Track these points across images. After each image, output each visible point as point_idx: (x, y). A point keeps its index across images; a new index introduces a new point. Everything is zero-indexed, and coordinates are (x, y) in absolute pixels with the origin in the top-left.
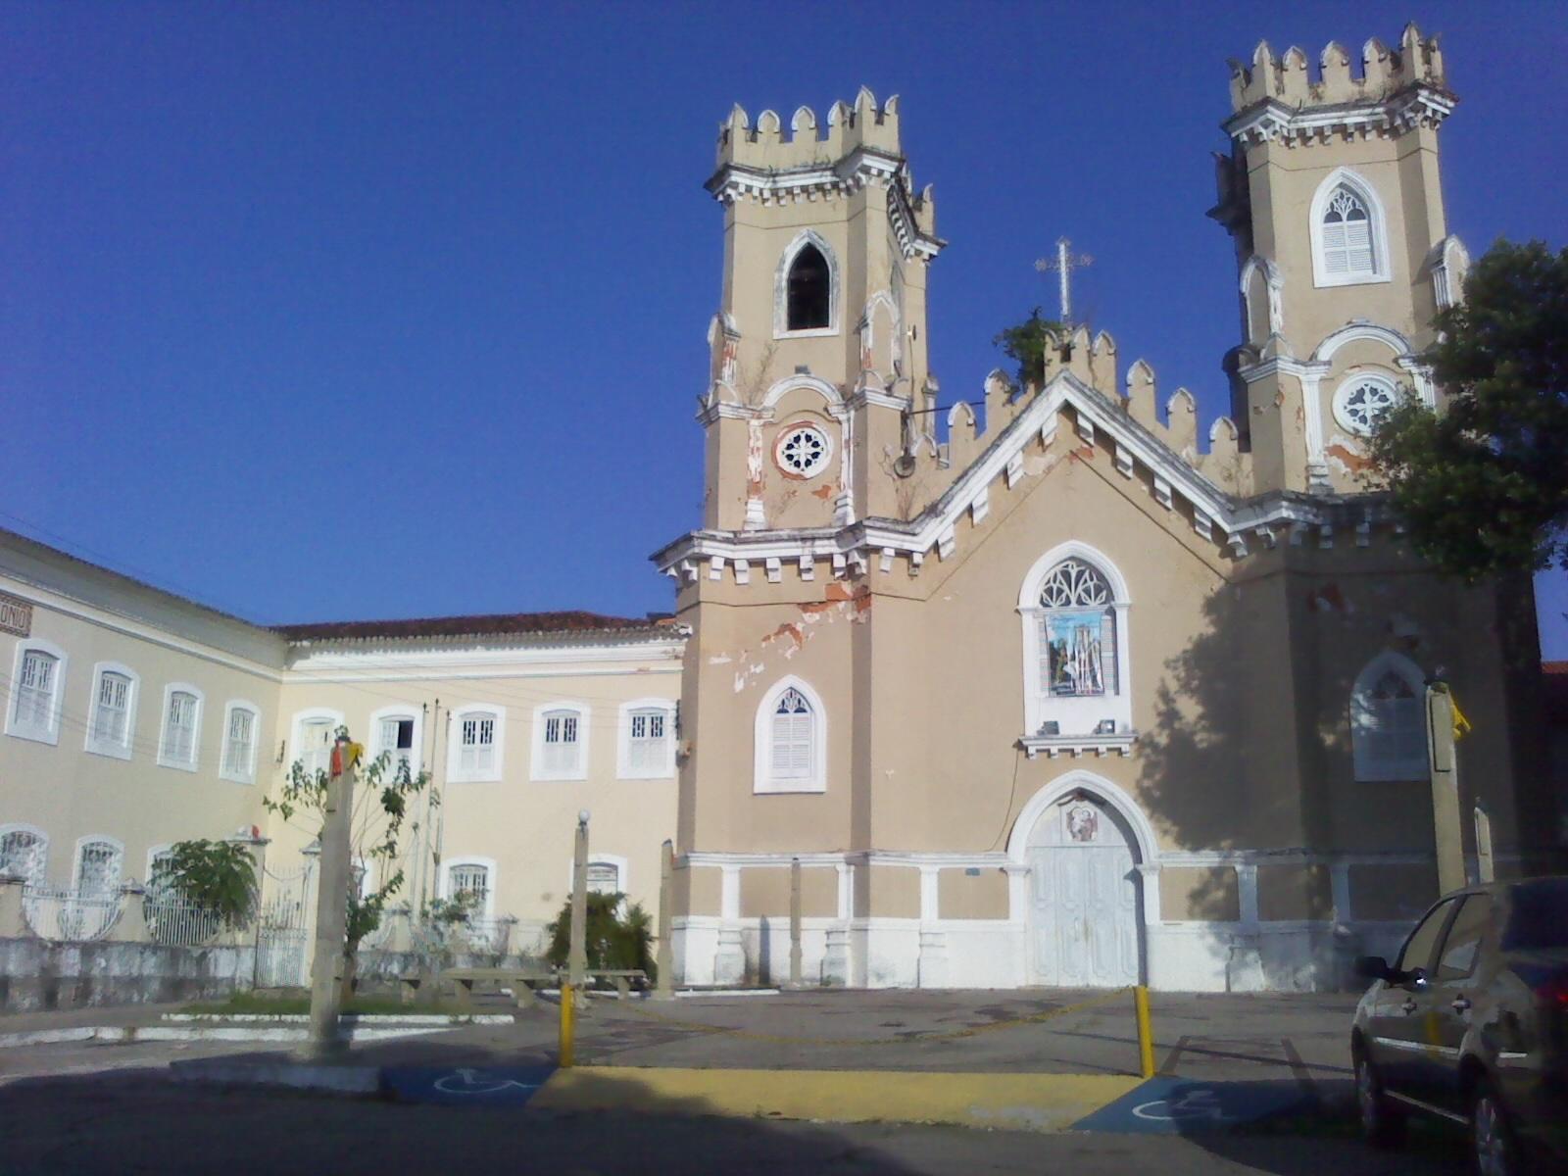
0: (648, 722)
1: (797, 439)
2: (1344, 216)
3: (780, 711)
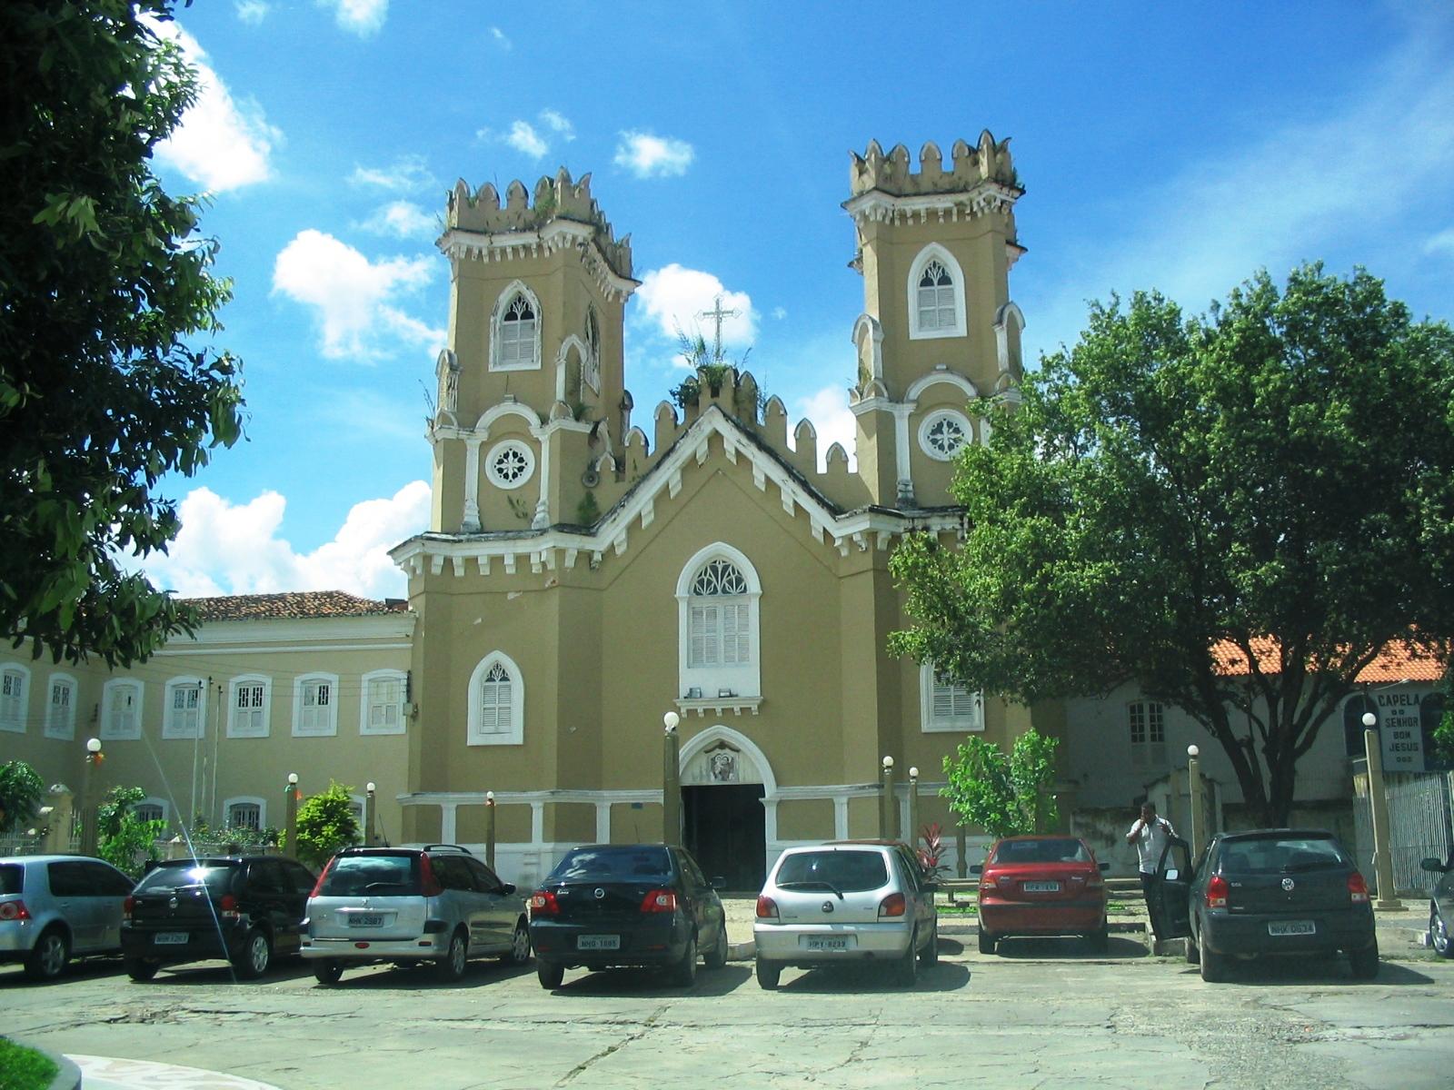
0: (251, 692)
1: (506, 456)
2: (936, 282)
3: (488, 680)
